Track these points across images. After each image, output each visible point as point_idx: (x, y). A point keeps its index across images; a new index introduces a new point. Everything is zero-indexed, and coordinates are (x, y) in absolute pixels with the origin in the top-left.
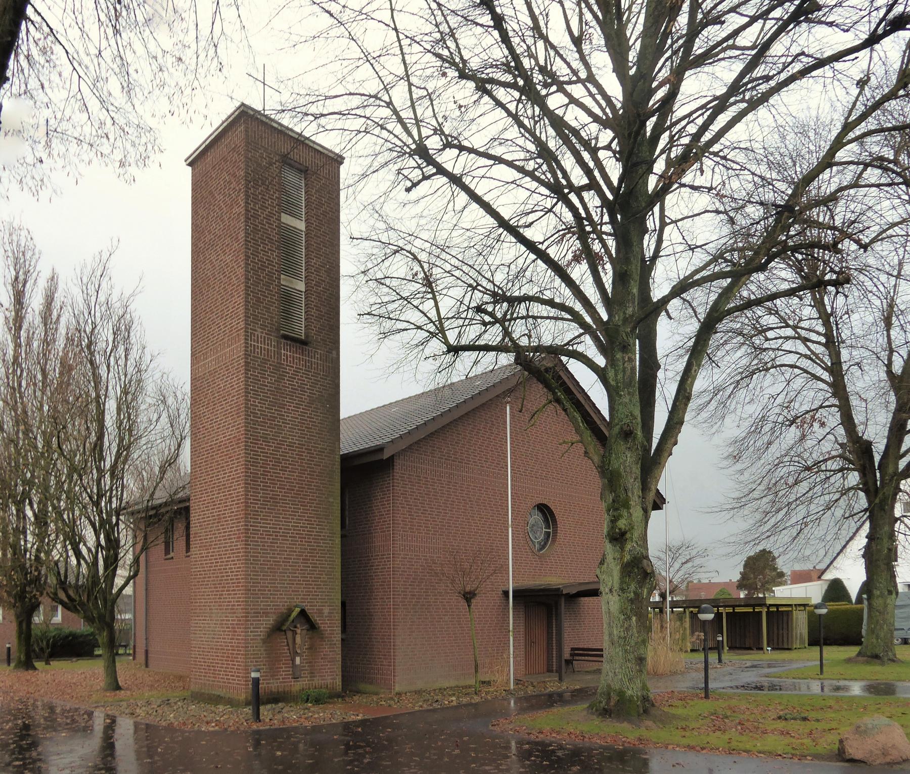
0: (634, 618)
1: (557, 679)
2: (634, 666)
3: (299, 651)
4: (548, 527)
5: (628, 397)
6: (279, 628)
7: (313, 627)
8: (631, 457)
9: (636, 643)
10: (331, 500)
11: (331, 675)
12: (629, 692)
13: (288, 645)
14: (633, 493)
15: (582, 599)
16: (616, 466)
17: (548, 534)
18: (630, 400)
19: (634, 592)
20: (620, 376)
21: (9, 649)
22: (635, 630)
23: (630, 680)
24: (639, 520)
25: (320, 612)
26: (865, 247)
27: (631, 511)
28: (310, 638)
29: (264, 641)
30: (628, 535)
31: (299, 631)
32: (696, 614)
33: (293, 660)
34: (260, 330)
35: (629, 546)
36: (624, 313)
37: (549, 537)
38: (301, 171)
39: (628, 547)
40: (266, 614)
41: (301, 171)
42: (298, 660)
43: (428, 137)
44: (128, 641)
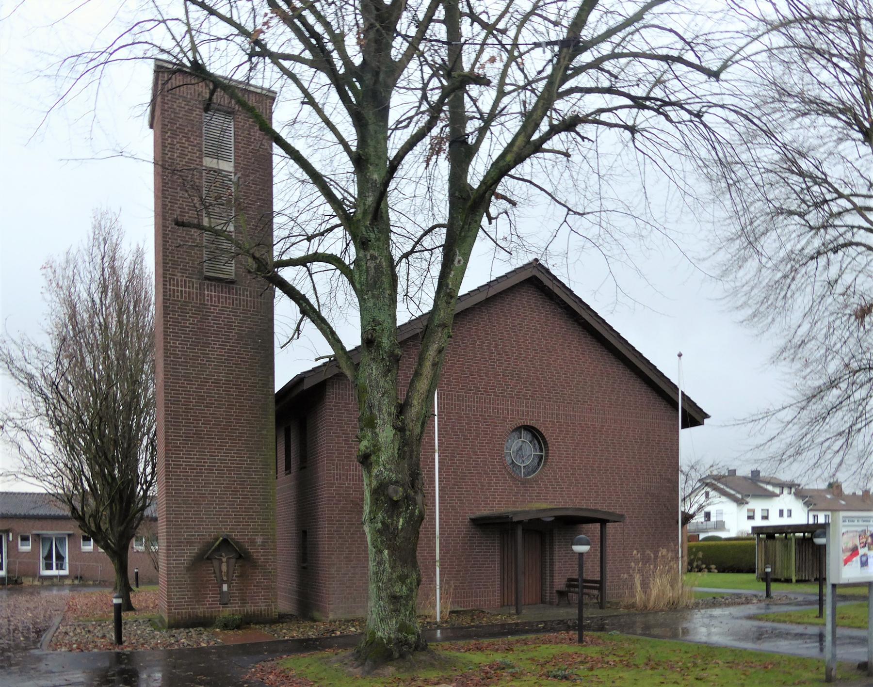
0: (386, 552)
1: (513, 611)
2: (387, 605)
3: (225, 579)
4: (541, 451)
5: (372, 301)
6: (207, 556)
7: (242, 557)
8: (377, 369)
9: (390, 580)
10: (264, 432)
11: (285, 605)
12: (380, 634)
13: (214, 573)
14: (380, 410)
15: (584, 525)
16: (362, 381)
17: (541, 457)
18: (375, 304)
19: (381, 522)
20: (364, 277)
21: (137, 573)
22: (387, 565)
23: (382, 620)
24: (389, 440)
25: (253, 542)
26: (715, 75)
27: (377, 430)
28: (241, 566)
29: (188, 569)
30: (373, 458)
31: (224, 560)
32: (811, 539)
33: (221, 587)
34: (179, 274)
35: (376, 471)
36: (364, 204)
37: (540, 461)
38: (229, 113)
39: (375, 471)
40: (190, 543)
41: (229, 113)
42: (225, 587)
43: (304, 50)
44: (799, 552)
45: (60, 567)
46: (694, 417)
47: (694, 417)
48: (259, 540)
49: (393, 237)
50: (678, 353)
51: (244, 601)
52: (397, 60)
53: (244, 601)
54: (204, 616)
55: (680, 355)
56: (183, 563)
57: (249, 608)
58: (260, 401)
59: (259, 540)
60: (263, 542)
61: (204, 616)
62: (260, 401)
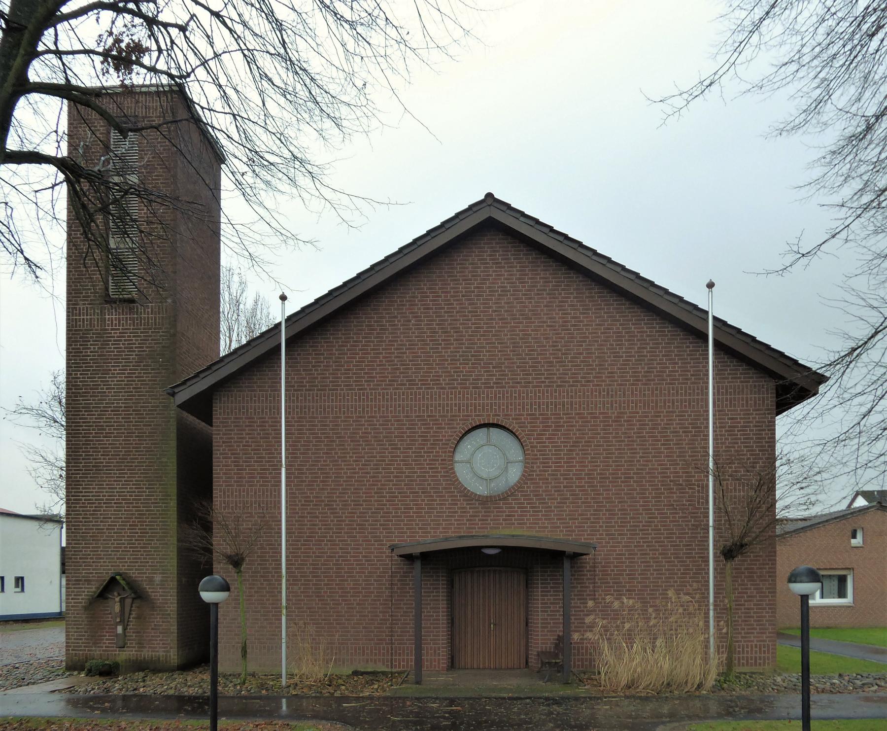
7: (138, 595)
10: (164, 460)
25: (151, 580)
29: (86, 608)
40: (89, 582)
45: (842, 594)
46: (793, 384)
47: (793, 384)
48: (158, 578)
49: (222, 238)
50: (708, 281)
51: (141, 645)
52: (65, 154)
53: (141, 645)
54: (137, 659)
55: (711, 285)
56: (81, 603)
57: (146, 654)
58: (160, 425)
59: (158, 578)
60: (162, 581)
61: (137, 659)
62: (160, 425)
